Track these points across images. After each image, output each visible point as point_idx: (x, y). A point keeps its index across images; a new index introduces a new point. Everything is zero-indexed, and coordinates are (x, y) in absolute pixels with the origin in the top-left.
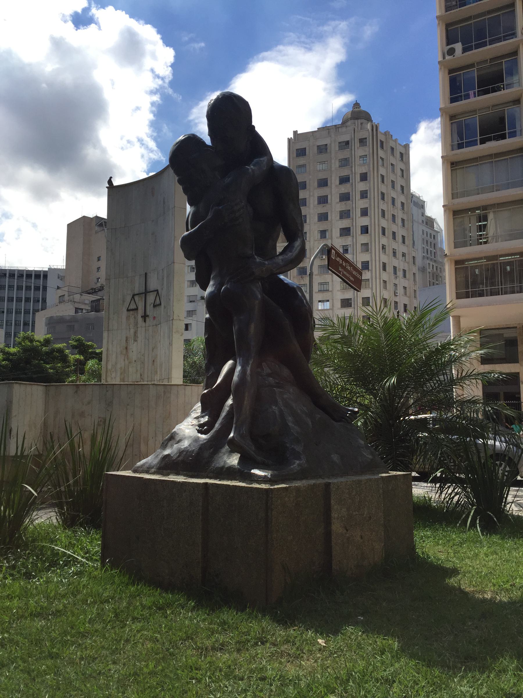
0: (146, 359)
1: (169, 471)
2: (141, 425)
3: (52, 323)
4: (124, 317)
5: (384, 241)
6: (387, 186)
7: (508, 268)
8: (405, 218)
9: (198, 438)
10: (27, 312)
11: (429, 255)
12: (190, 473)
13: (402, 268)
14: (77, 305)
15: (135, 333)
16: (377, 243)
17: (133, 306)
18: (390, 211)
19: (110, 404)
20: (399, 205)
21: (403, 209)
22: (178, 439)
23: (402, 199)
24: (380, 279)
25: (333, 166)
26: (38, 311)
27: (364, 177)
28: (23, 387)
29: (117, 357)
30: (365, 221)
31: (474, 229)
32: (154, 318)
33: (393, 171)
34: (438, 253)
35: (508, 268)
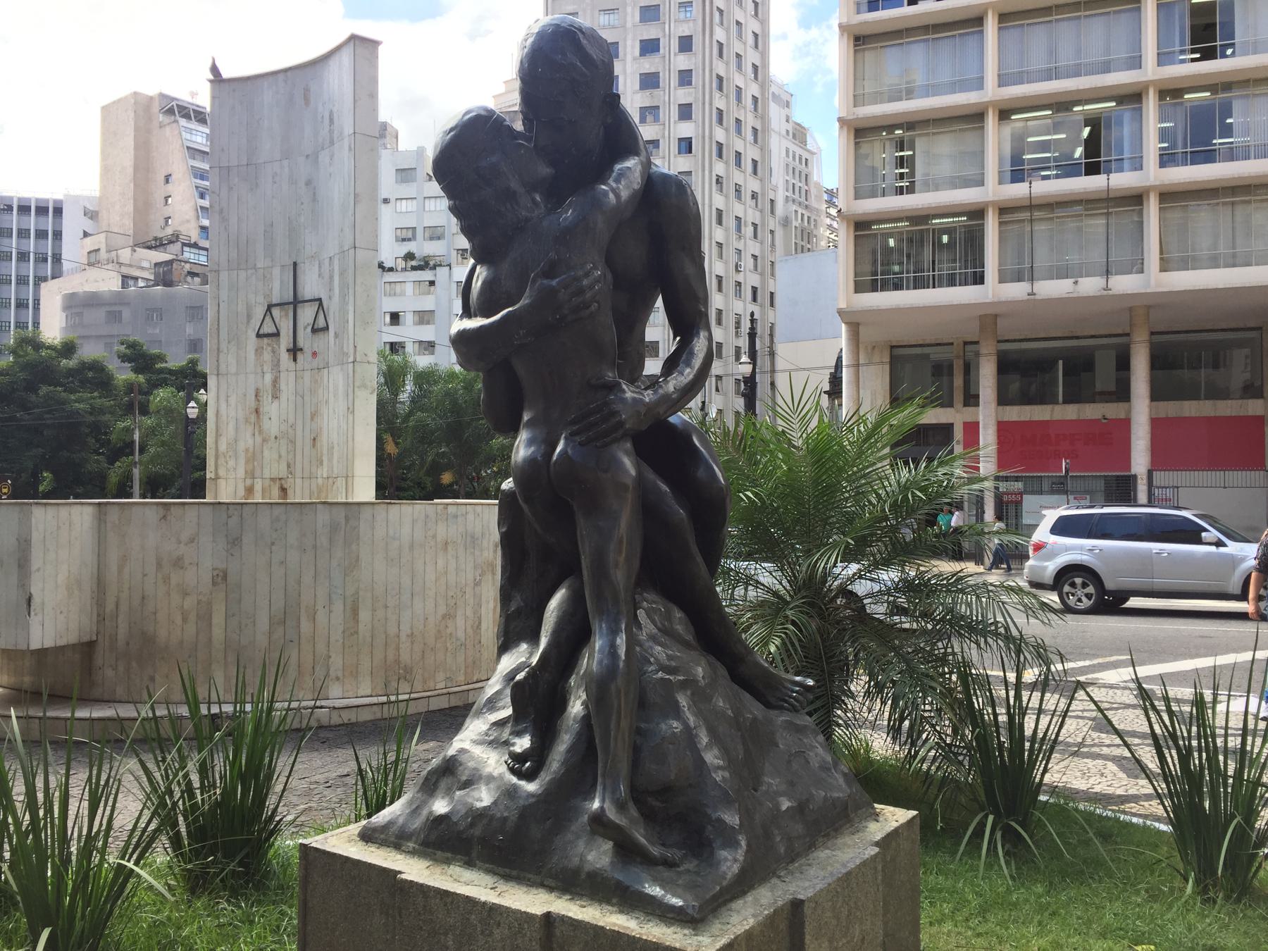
0: (299, 433)
1: (449, 855)
2: (299, 583)
3: (76, 305)
4: (251, 355)
5: (719, 168)
6: (727, 64)
7: (945, 239)
8: (759, 127)
9: (515, 788)
10: (22, 281)
11: (796, 196)
12: (501, 870)
13: (750, 220)
14: (125, 270)
15: (275, 382)
16: (707, 172)
17: (268, 328)
18: (734, 112)
19: (235, 542)
20: (749, 102)
21: (756, 109)
22: (464, 778)
23: (753, 89)
24: (711, 239)
25: (629, 19)
26: (45, 279)
27: (686, 44)
28: (51, 511)
29: (237, 429)
30: (686, 129)
31: (890, 163)
32: (315, 354)
33: (740, 35)
34: (813, 191)
35: (945, 239)
